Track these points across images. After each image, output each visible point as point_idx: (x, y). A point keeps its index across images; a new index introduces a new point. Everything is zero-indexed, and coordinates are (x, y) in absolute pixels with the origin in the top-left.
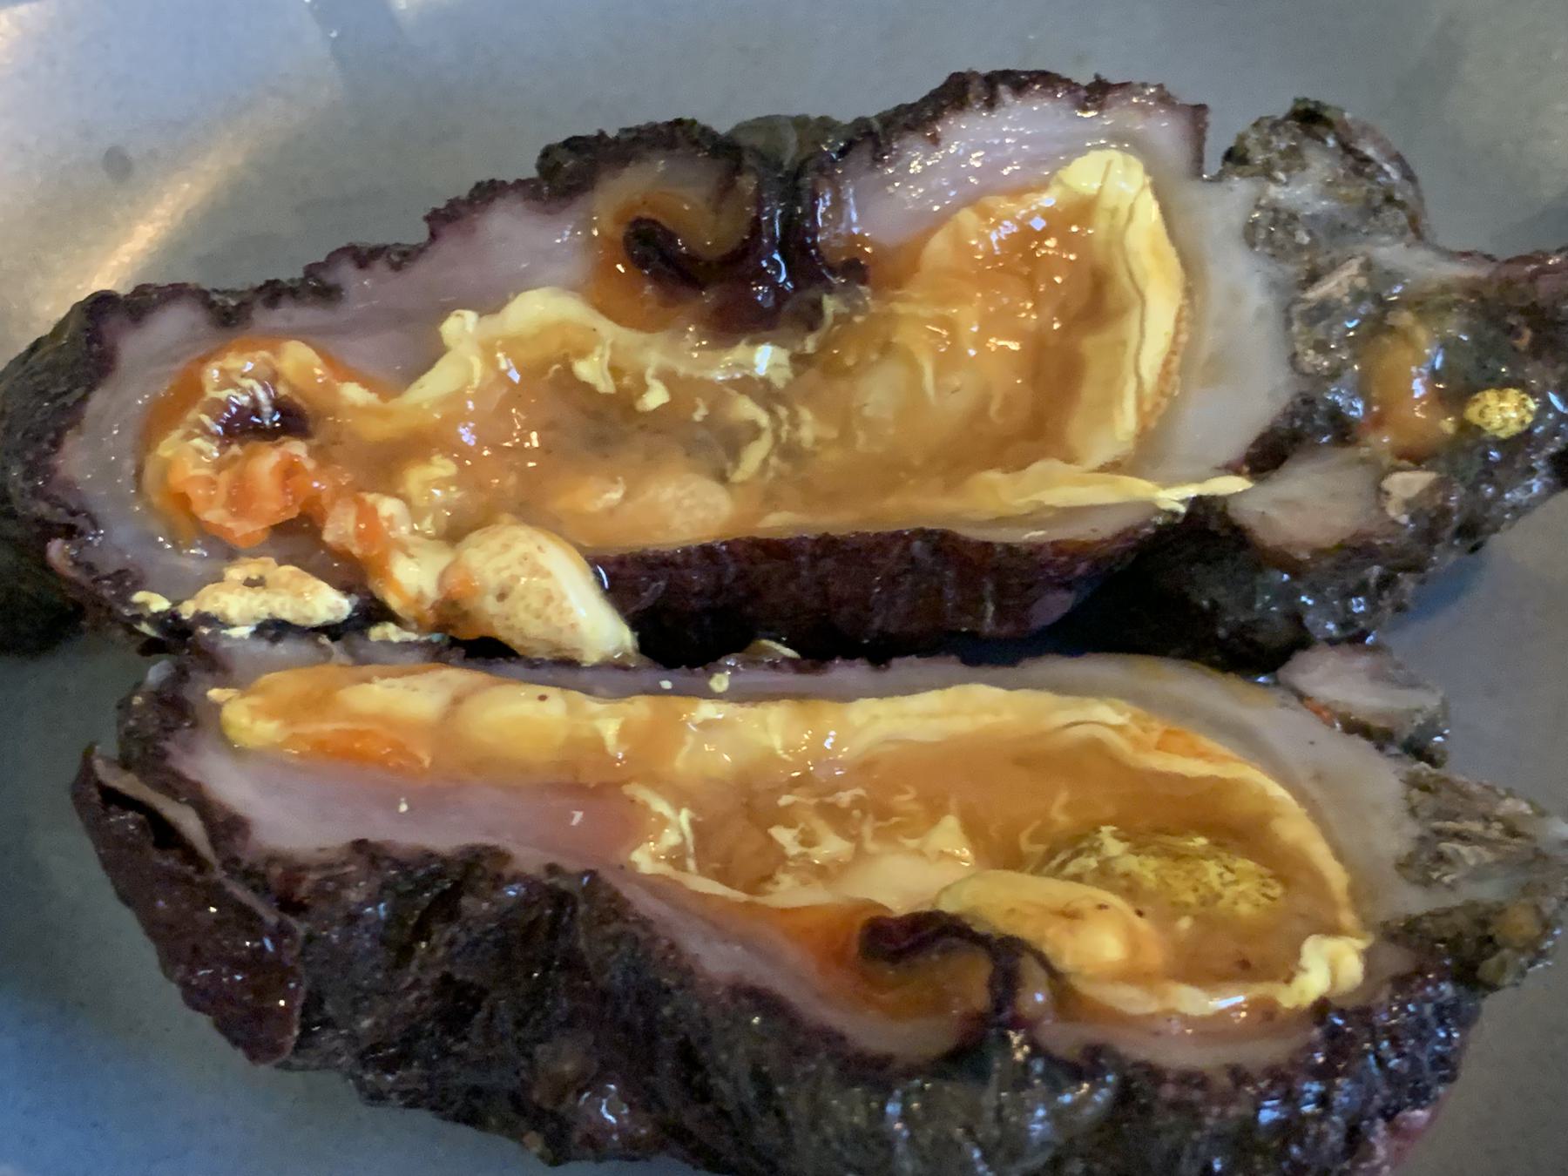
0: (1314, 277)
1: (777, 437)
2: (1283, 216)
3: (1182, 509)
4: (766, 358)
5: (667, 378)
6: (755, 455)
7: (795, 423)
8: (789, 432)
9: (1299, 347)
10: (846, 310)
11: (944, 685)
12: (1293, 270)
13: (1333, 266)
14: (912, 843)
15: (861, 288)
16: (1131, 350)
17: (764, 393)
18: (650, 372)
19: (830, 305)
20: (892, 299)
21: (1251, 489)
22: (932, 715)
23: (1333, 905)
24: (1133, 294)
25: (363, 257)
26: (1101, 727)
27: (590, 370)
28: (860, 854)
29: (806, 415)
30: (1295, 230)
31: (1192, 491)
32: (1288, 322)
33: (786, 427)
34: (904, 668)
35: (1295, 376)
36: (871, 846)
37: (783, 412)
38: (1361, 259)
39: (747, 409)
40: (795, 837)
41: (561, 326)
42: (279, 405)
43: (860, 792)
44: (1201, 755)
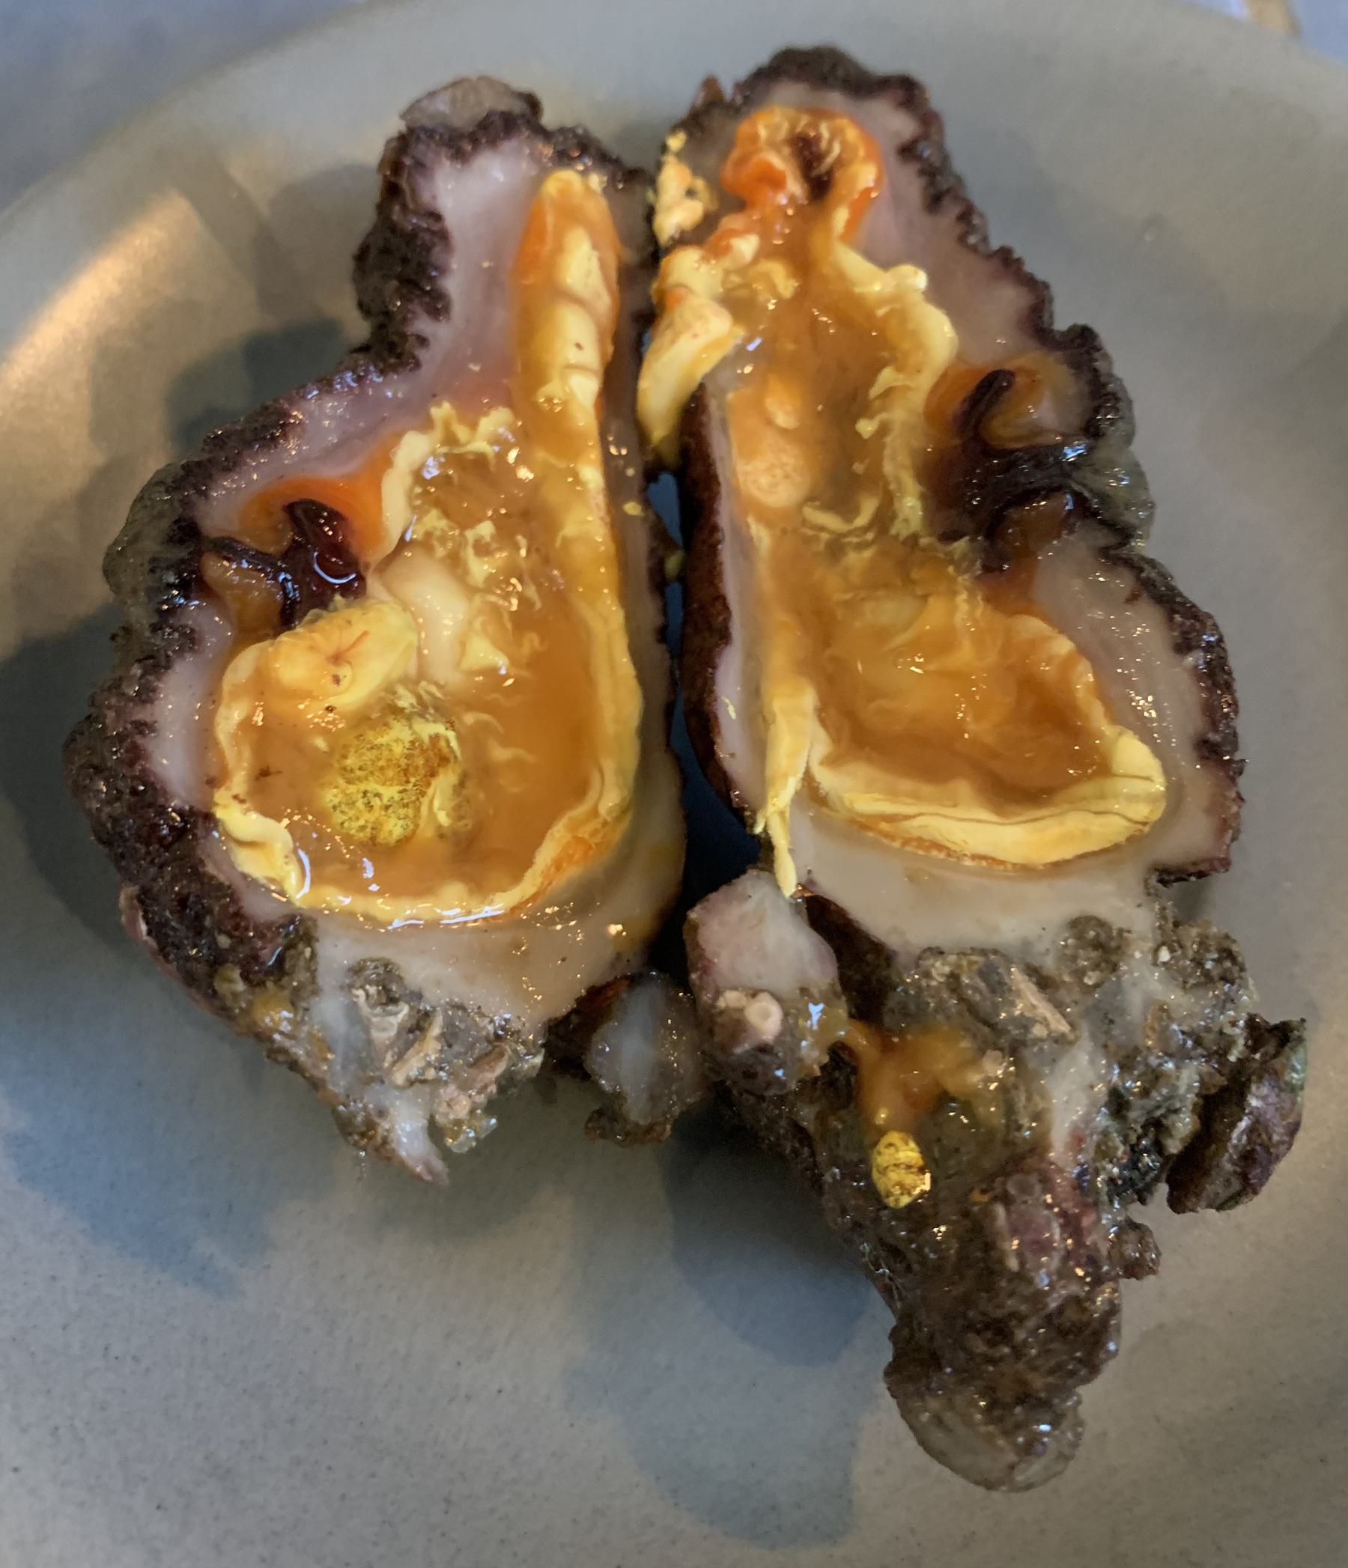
0: (1044, 983)
1: (850, 533)
2: (1114, 958)
3: (758, 830)
4: (911, 507)
5: (883, 430)
6: (832, 522)
7: (860, 547)
8: (850, 543)
9: (952, 958)
10: (956, 557)
11: (642, 678)
12: (1049, 964)
13: (1059, 1006)
14: (477, 624)
15: (978, 564)
16: (950, 811)
17: (884, 519)
18: (884, 416)
19: (961, 545)
20: (972, 595)
21: (783, 897)
22: (613, 668)
23: (510, 1058)
24: (1012, 821)
25: (966, 215)
26: (597, 796)
27: (887, 377)
28: (471, 590)
29: (868, 554)
30: (1101, 971)
31: (781, 841)
32: (983, 952)
33: (855, 540)
34: (658, 653)
35: (918, 952)
36: (478, 600)
37: (870, 536)
38: (1071, 1037)
39: (868, 507)
40: (482, 537)
41: (920, 345)
42: (830, 173)
43: (538, 605)
44: (558, 865)
